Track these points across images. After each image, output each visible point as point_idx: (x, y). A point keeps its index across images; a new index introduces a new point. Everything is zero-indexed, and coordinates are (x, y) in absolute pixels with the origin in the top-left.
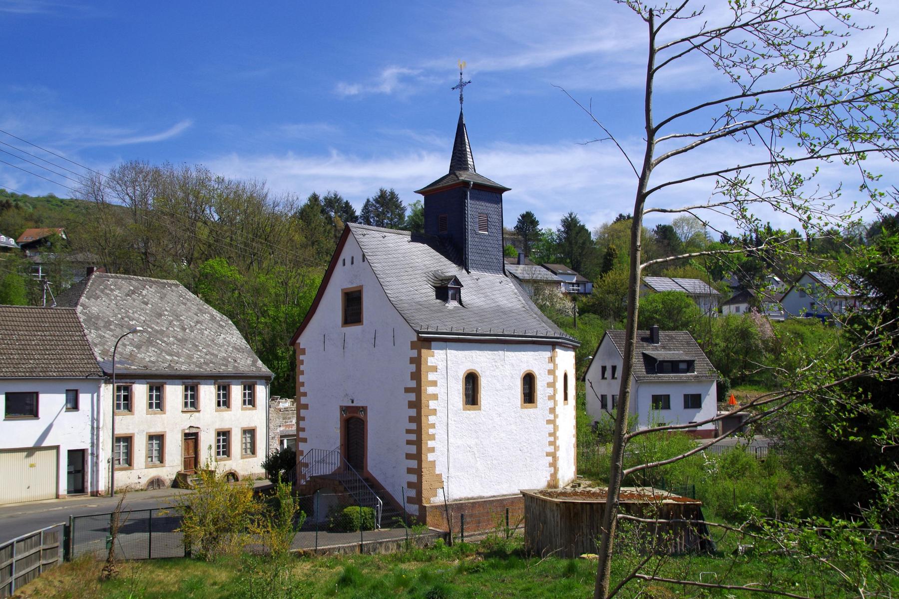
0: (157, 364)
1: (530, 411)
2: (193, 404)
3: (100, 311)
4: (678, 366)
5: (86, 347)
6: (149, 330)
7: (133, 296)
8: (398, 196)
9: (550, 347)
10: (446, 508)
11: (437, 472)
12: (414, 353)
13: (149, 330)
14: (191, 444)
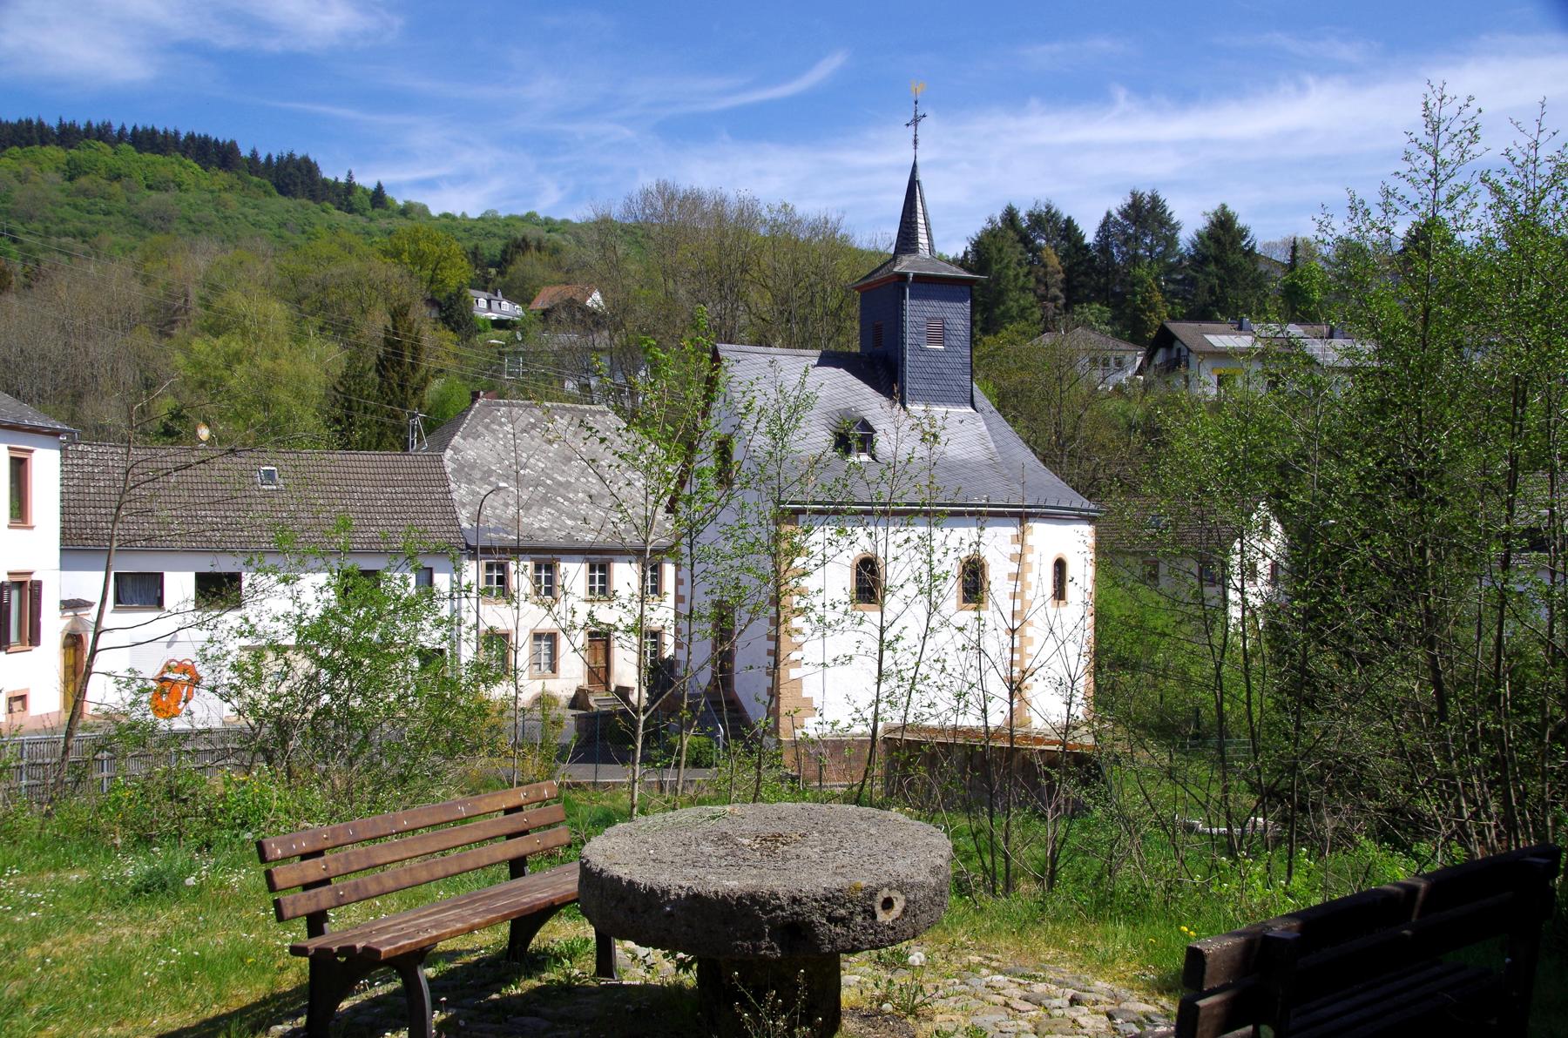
0: (549, 532)
2: (603, 590)
3: (479, 456)
5: (448, 508)
6: (549, 482)
7: (533, 432)
8: (1166, 203)
9: (1016, 520)
10: (796, 744)
13: (549, 482)
14: (600, 646)
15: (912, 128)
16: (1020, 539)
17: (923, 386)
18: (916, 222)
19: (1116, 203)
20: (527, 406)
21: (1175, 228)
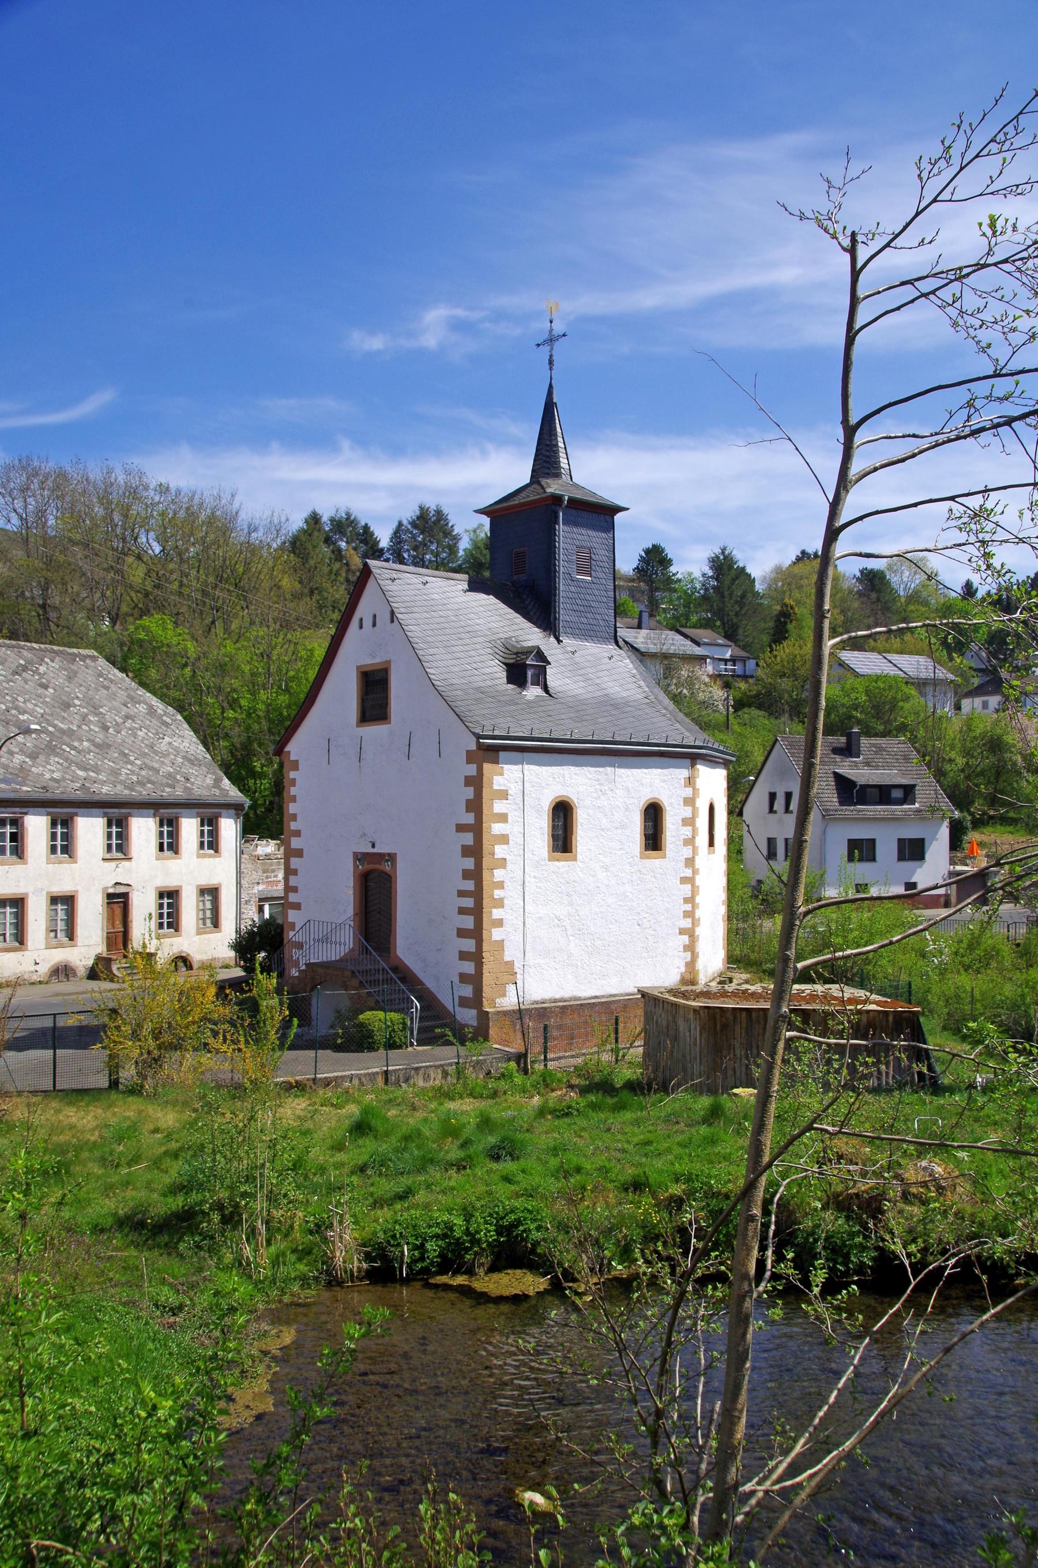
1: (654, 863)
2: (120, 848)
4: (890, 793)
6: (51, 729)
7: (24, 674)
8: (449, 517)
9: (688, 762)
11: (507, 958)
12: (472, 770)
13: (51, 729)
14: (118, 911)
15: (546, 349)
16: (690, 781)
17: (573, 619)
18: (557, 445)
19: (408, 513)
20: (13, 647)
21: (456, 539)
